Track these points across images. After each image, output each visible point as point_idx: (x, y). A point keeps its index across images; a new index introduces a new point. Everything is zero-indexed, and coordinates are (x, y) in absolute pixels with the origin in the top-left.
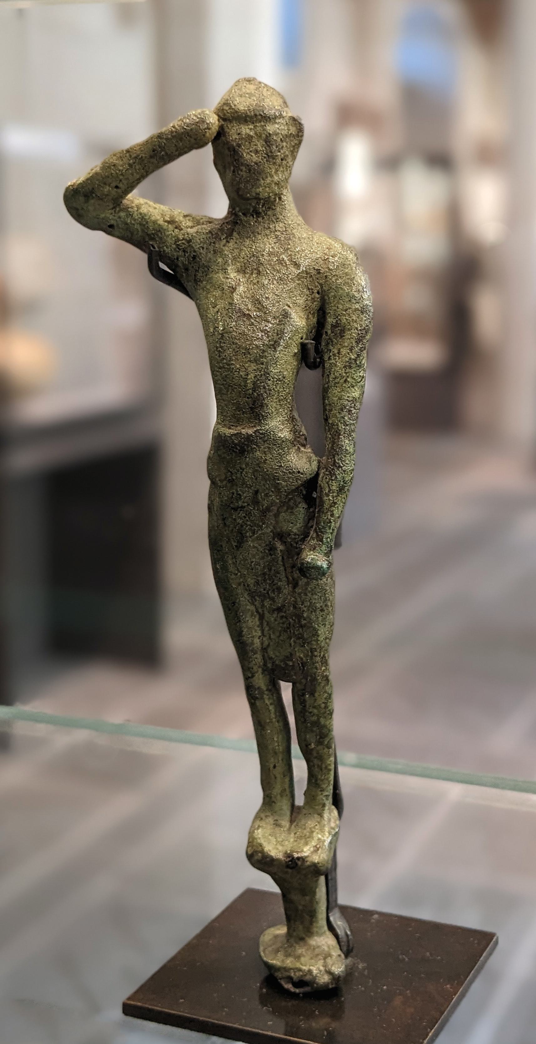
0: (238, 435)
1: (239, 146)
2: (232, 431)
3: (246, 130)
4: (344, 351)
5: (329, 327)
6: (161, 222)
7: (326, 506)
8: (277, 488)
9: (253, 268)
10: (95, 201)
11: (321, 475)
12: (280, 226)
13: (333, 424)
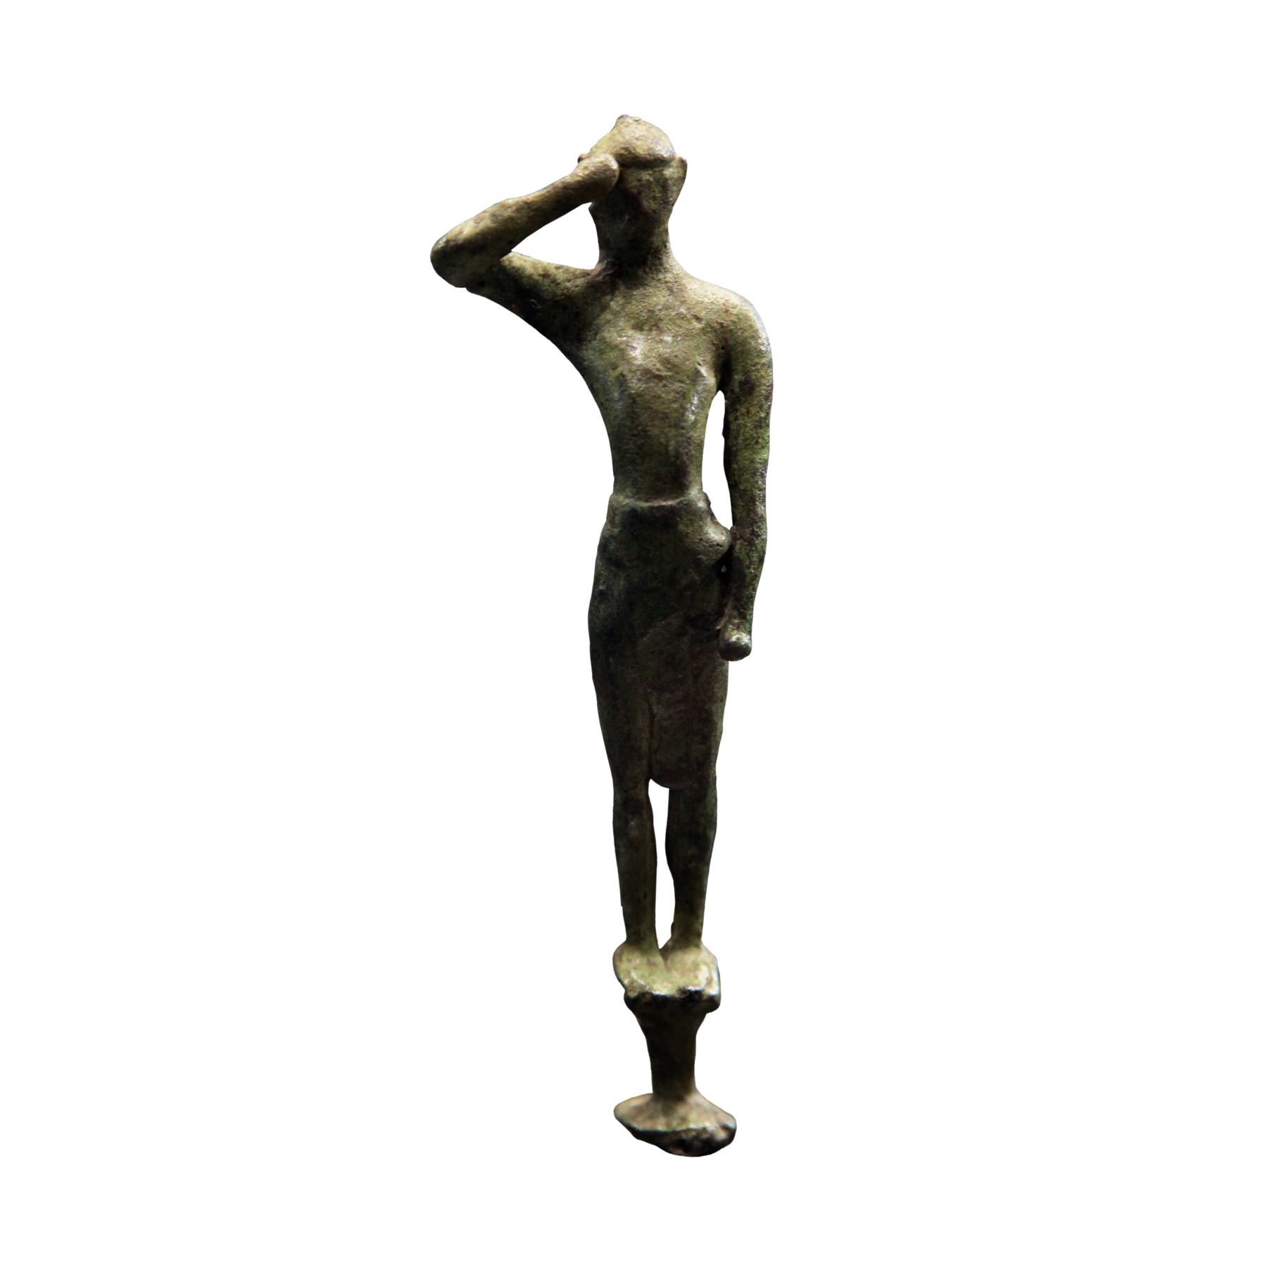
0: (652, 508)
1: (640, 193)
2: (645, 505)
3: (646, 176)
4: (753, 410)
5: (737, 384)
6: (536, 277)
7: (748, 579)
8: (698, 564)
9: (648, 323)
10: (477, 261)
11: (738, 547)
12: (669, 277)
13: (745, 490)
